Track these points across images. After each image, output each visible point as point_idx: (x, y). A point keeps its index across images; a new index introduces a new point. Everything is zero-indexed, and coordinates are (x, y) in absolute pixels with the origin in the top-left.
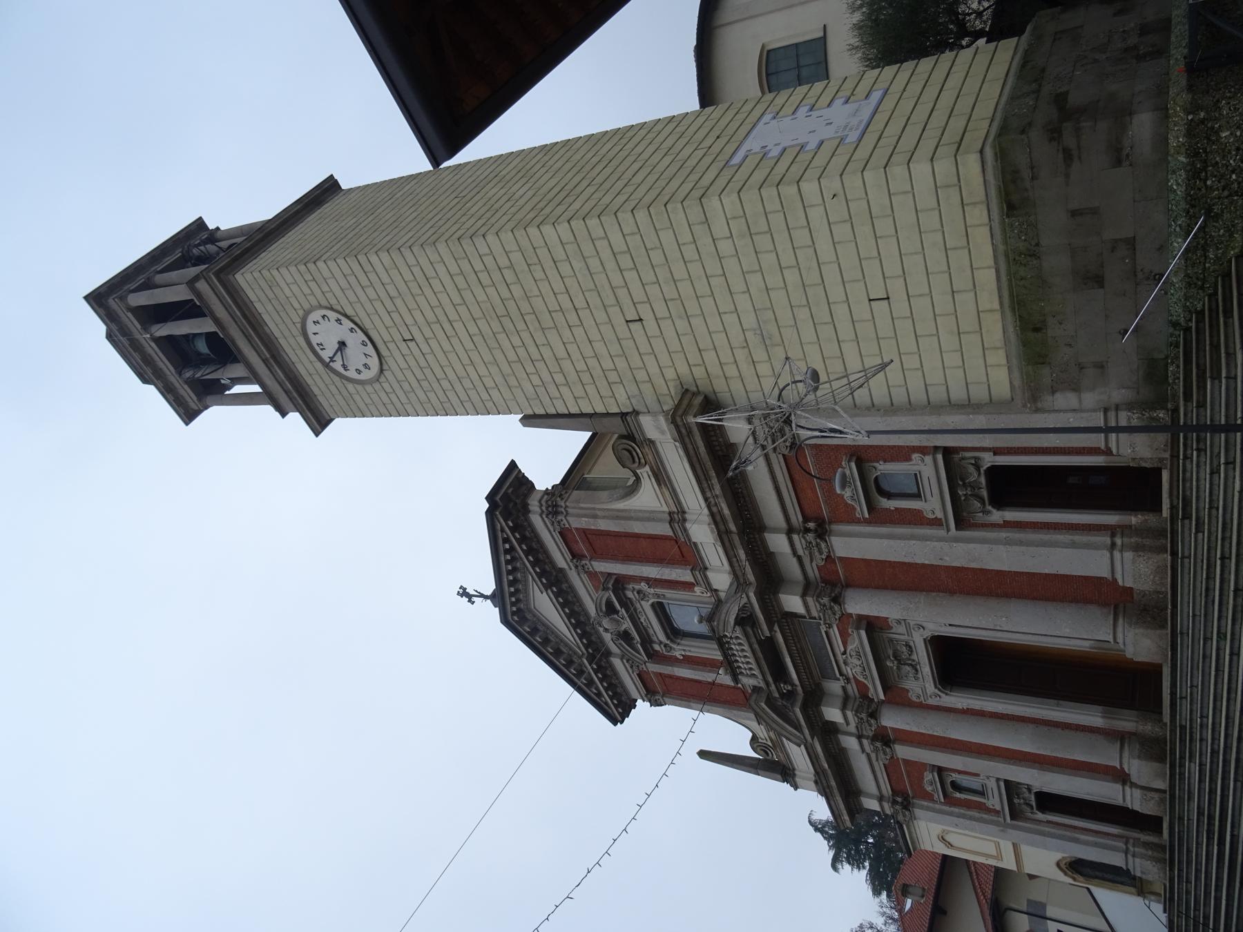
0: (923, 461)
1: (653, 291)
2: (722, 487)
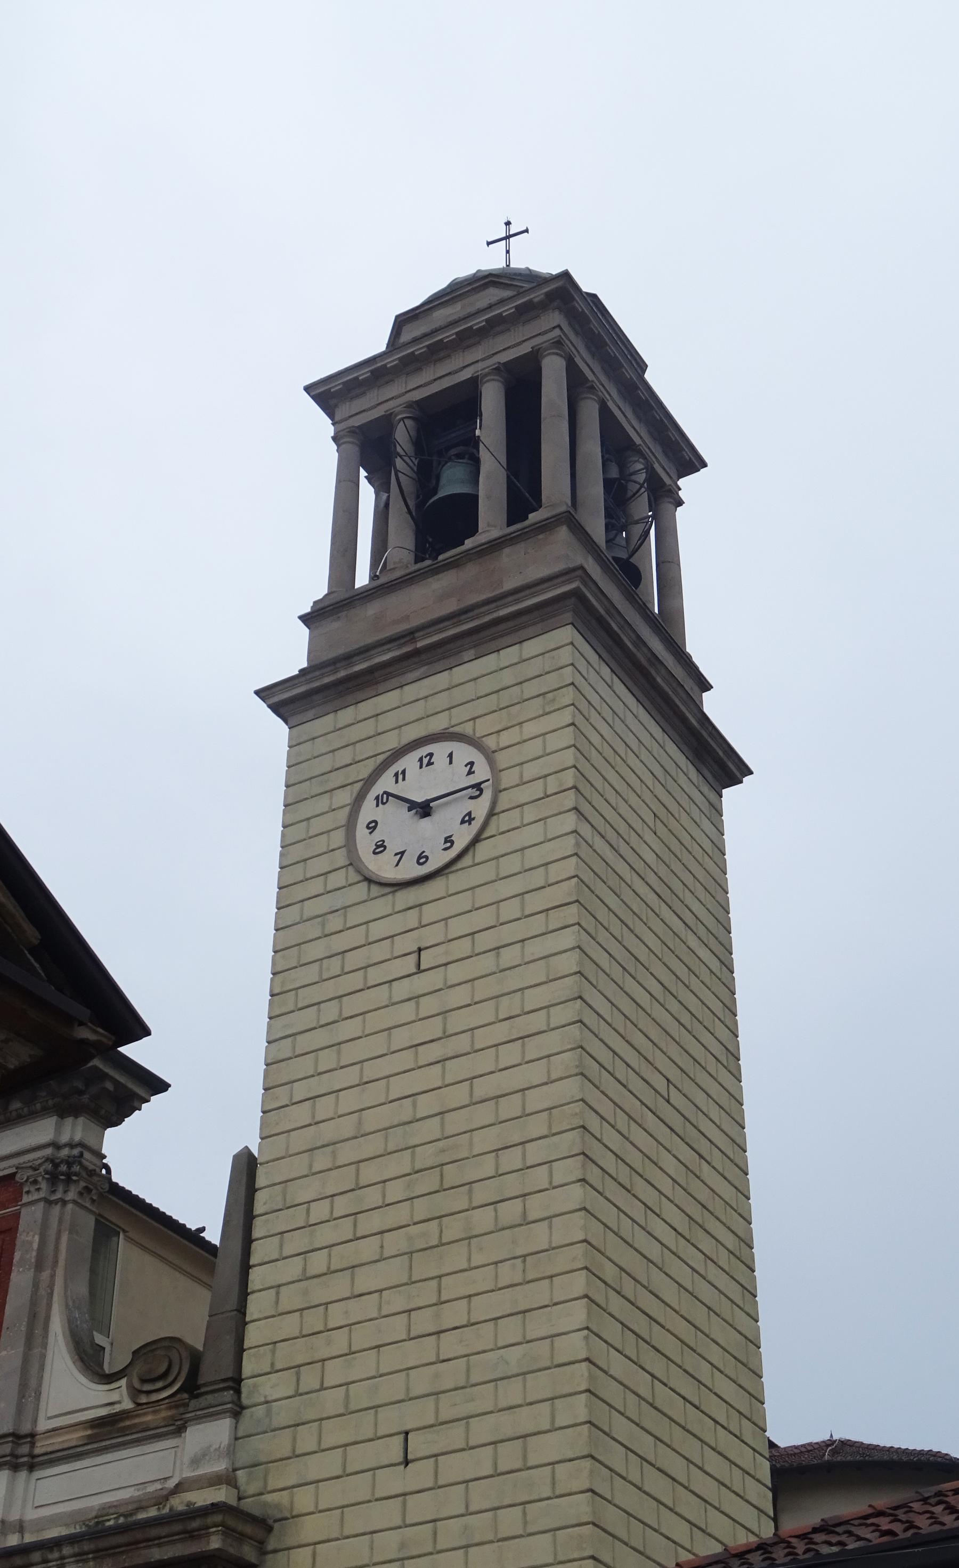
1: (454, 1500)
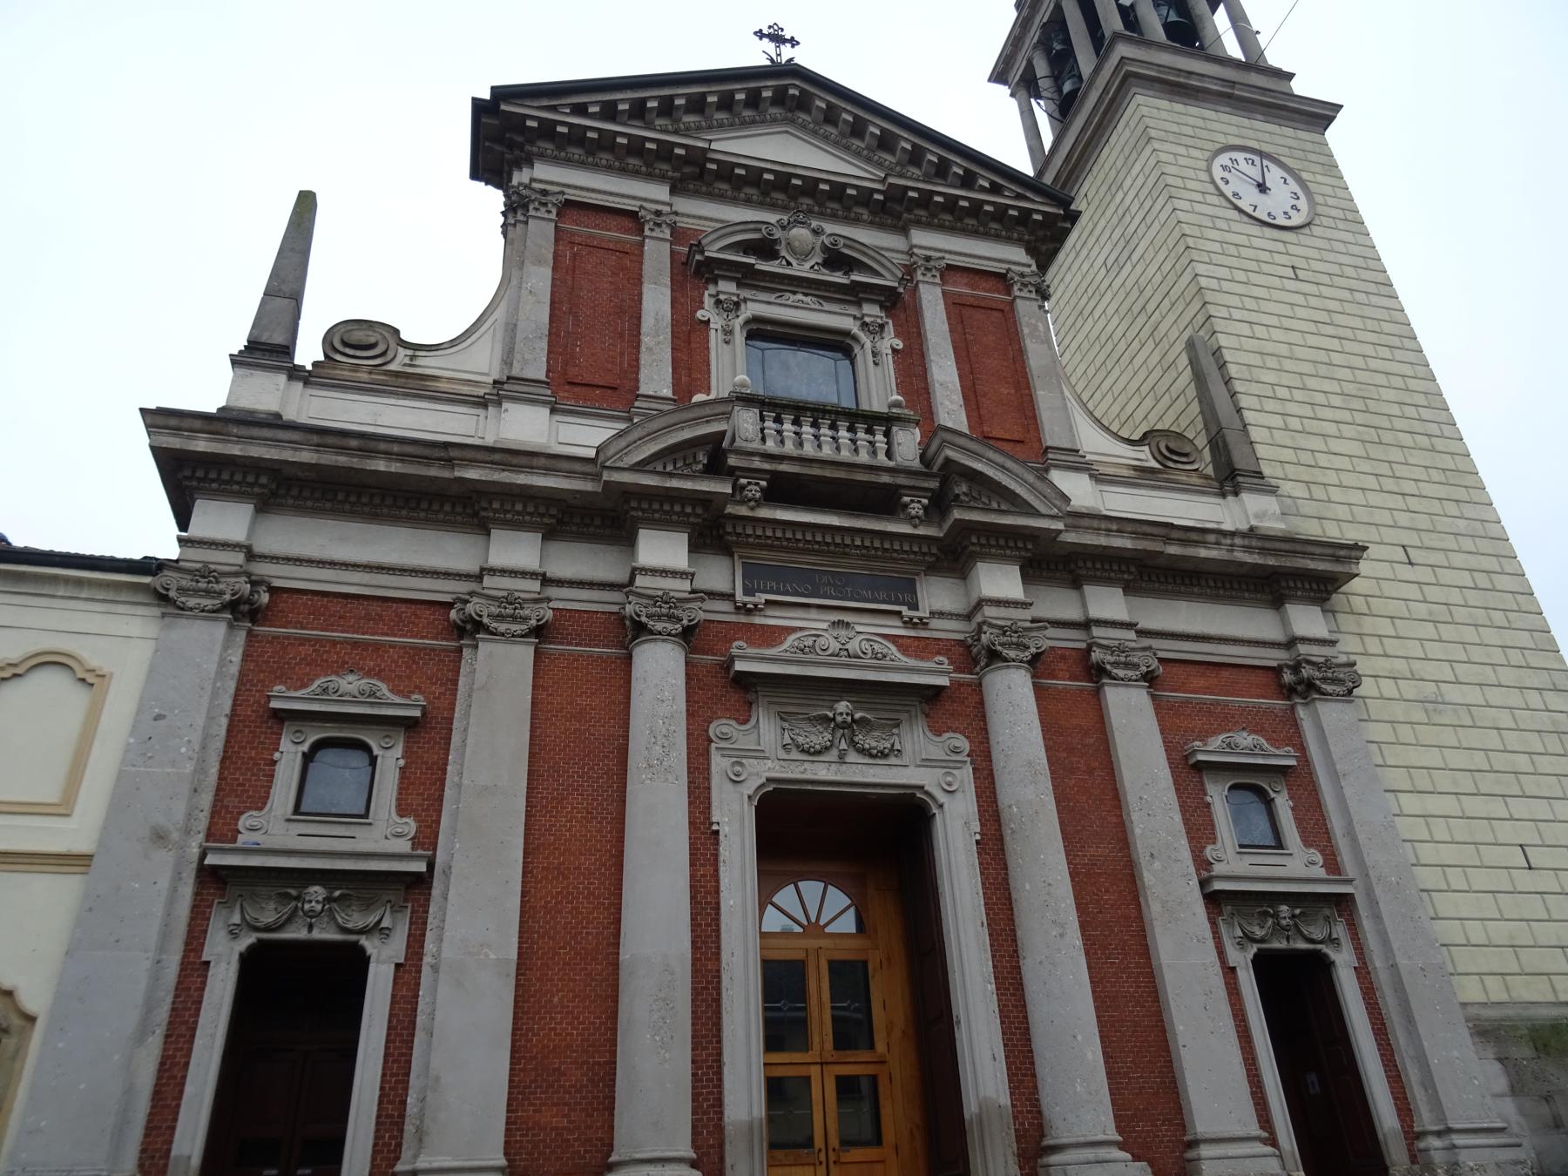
0: (398, 836)
2: (1242, 564)
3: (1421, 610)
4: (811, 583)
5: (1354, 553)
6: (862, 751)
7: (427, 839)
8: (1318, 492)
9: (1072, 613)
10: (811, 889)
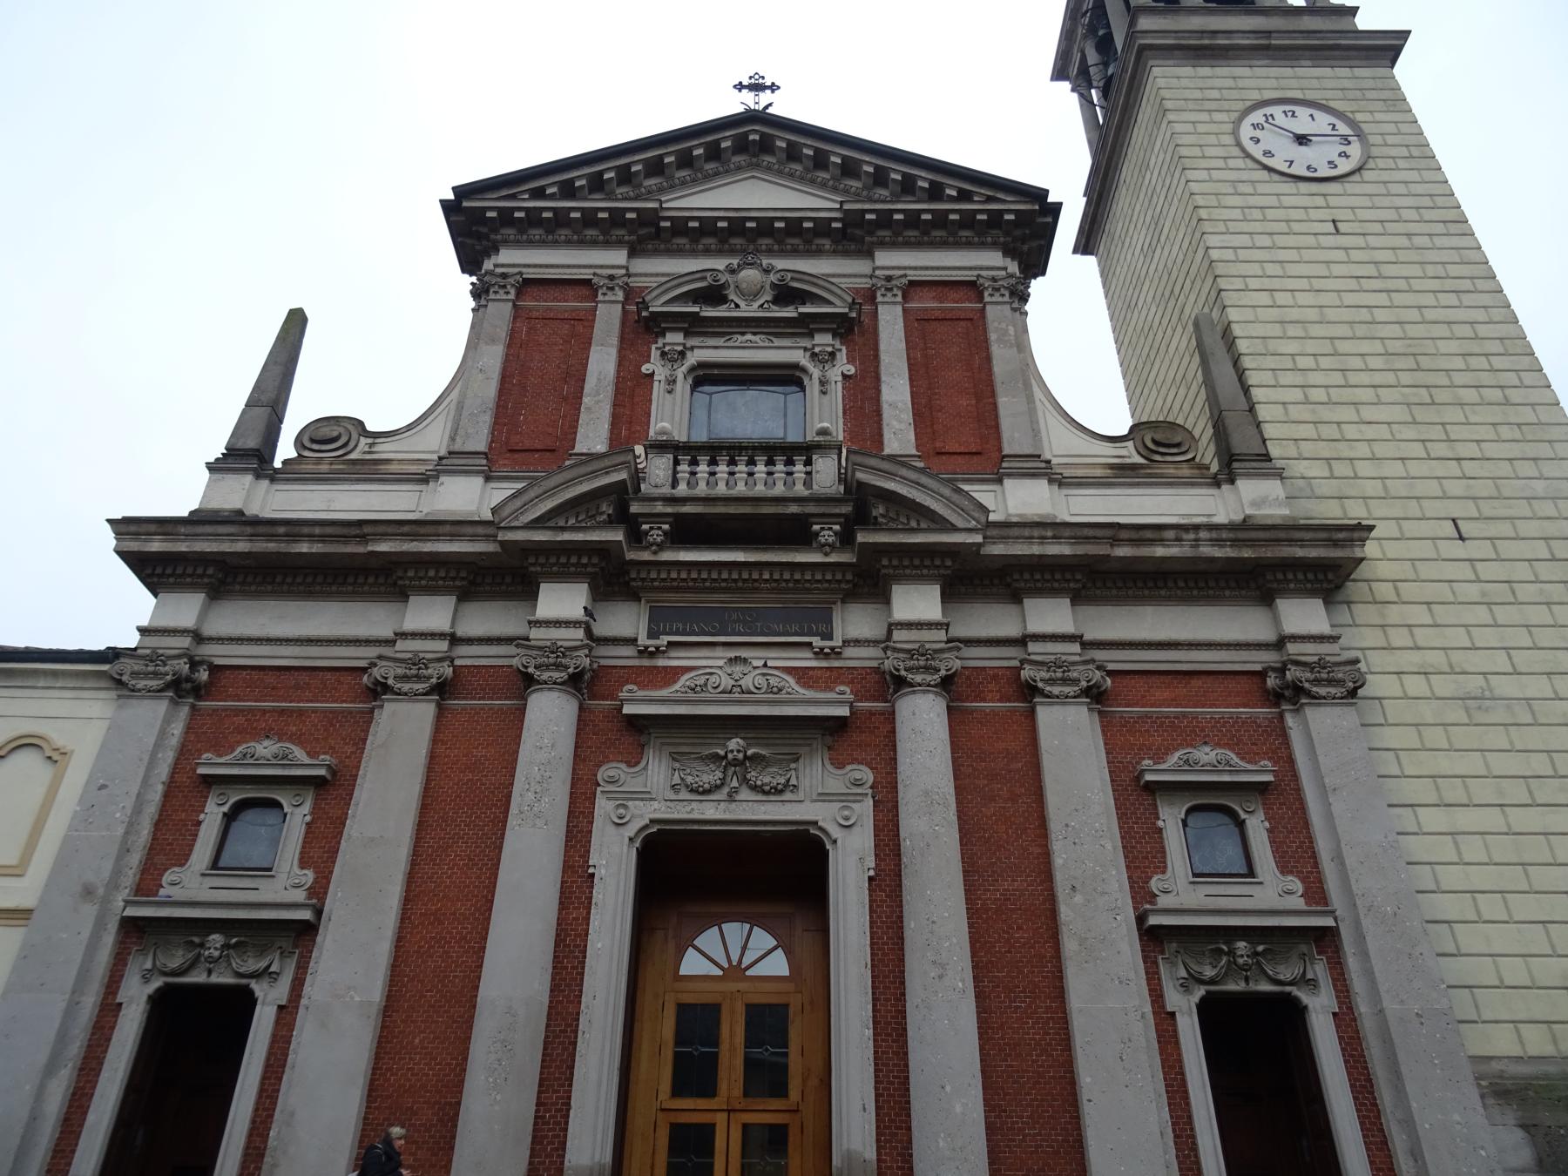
0: (296, 886)
2: (1213, 560)
3: (1472, 591)
4: (718, 622)
5: (1356, 535)
6: (755, 788)
7: (318, 892)
8: (1341, 469)
9: (1011, 630)
10: (734, 931)
